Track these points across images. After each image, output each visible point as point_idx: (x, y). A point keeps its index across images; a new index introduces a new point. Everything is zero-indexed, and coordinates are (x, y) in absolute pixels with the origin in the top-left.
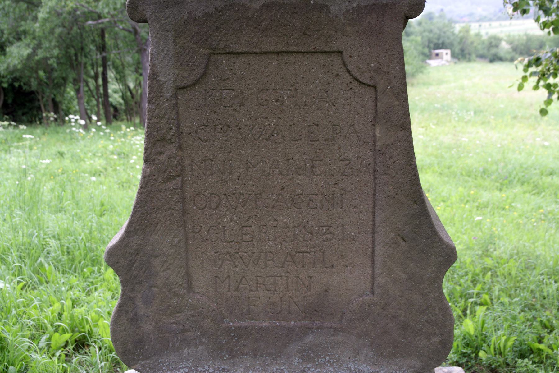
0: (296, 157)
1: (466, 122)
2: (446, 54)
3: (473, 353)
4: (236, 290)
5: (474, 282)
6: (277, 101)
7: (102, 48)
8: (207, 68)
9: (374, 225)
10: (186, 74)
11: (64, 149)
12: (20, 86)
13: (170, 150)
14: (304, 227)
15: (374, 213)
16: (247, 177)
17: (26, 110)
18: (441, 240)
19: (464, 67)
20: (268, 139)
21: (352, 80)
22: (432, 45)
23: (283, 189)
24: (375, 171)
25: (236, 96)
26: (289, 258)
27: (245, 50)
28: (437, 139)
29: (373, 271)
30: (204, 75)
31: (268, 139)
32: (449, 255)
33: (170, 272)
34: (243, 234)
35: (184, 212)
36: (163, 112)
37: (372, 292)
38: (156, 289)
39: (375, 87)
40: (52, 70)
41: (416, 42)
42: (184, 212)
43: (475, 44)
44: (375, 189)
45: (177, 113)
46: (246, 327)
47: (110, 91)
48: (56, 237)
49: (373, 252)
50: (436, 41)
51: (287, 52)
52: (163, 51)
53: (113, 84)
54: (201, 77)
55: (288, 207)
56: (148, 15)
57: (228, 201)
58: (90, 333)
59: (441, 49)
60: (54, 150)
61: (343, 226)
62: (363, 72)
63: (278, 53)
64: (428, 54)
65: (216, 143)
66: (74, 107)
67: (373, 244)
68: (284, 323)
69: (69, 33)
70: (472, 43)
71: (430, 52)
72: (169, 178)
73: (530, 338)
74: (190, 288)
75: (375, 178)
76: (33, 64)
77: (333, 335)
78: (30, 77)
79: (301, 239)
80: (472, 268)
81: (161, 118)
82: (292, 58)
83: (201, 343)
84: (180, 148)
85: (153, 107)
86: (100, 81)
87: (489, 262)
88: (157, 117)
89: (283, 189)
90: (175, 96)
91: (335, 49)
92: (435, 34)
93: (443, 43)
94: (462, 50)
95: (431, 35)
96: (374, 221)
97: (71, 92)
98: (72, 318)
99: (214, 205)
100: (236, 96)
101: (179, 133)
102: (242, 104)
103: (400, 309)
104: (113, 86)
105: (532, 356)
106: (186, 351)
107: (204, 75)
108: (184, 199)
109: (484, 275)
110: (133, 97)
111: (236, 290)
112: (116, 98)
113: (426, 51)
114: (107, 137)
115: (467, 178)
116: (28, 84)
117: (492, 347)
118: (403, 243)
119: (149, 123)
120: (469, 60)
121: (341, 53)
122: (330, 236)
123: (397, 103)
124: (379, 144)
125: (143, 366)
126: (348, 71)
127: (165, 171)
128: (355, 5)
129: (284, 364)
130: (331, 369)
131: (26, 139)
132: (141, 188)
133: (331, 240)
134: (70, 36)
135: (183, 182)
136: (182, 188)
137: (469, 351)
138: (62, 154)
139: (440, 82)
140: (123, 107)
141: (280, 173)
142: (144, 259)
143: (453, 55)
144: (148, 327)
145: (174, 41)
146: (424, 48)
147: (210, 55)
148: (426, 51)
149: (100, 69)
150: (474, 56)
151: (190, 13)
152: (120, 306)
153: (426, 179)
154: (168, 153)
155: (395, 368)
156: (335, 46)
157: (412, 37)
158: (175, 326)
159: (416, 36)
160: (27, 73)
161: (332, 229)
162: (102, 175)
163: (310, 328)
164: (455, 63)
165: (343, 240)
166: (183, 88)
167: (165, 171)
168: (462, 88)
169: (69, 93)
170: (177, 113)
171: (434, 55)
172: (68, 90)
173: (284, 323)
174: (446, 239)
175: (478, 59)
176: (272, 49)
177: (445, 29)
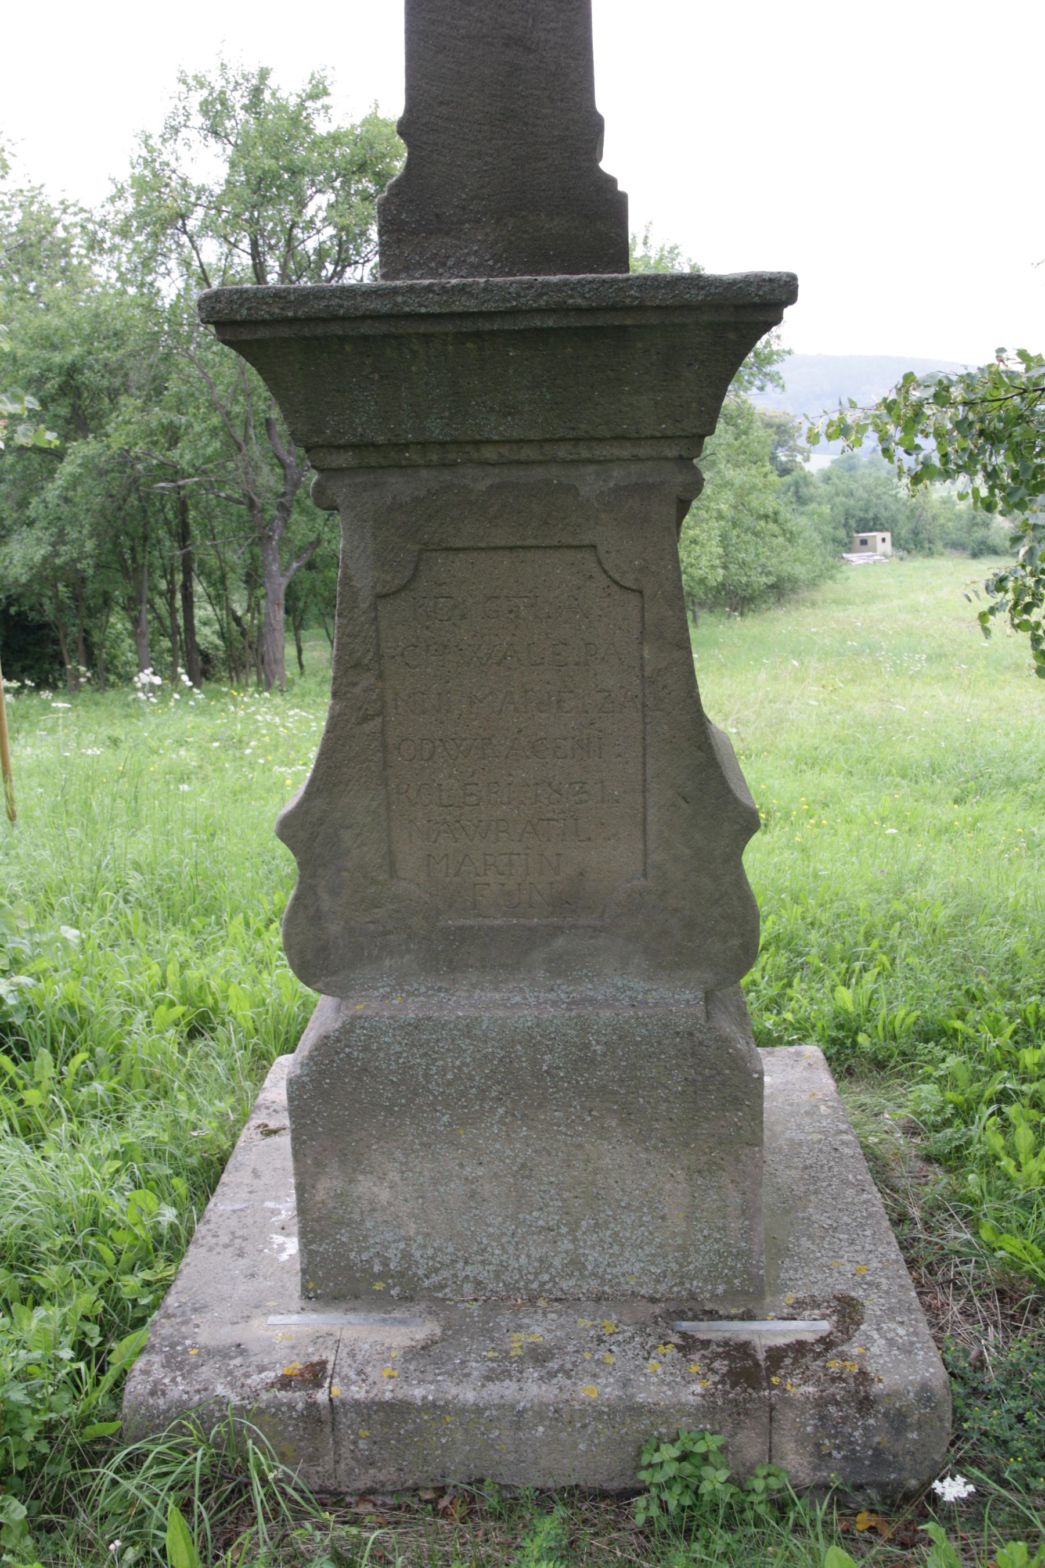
0: (538, 688)
1: (911, 677)
2: (881, 541)
3: (847, 1037)
4: (457, 874)
5: (868, 937)
6: (510, 612)
7: (183, 535)
8: (416, 568)
9: (645, 780)
10: (388, 578)
11: (119, 732)
12: (19, 614)
13: (367, 680)
14: (550, 784)
15: (644, 763)
16: (473, 716)
17: (28, 662)
18: (736, 800)
19: (917, 566)
20: (499, 664)
21: (610, 583)
22: (852, 523)
23: (520, 731)
24: (644, 705)
25: (455, 607)
26: (529, 828)
27: (467, 545)
28: (850, 708)
29: (645, 845)
30: (413, 578)
31: (499, 664)
32: (748, 823)
33: (365, 849)
34: (466, 795)
35: (386, 766)
36: (358, 628)
37: (645, 876)
38: (345, 874)
39: (641, 592)
40: (83, 580)
41: (820, 515)
42: (386, 766)
43: (942, 521)
44: (644, 731)
45: (377, 630)
46: (472, 927)
47: (196, 622)
48: (137, 867)
49: (645, 819)
50: (861, 514)
51: (523, 547)
52: (358, 547)
53: (200, 608)
54: (409, 582)
55: (528, 757)
56: (339, 501)
57: (445, 749)
58: (215, 1009)
59: (871, 531)
60: (105, 732)
61: (602, 782)
62: (624, 573)
63: (511, 549)
64: (846, 540)
65: (429, 670)
66: (123, 654)
67: (644, 807)
68: (523, 921)
69: (120, 509)
70: (935, 518)
71: (849, 536)
72: (366, 718)
73: (941, 1011)
74: (393, 872)
75: (645, 716)
76: (49, 572)
77: (591, 937)
78: (41, 595)
79: (546, 802)
80: (868, 916)
81: (356, 637)
82: (530, 555)
83: (408, 951)
84: (380, 676)
85: (345, 621)
86: (179, 603)
87: (899, 906)
88: (349, 636)
89: (520, 731)
90: (374, 607)
91: (586, 542)
92: (860, 499)
93: (876, 519)
94: (916, 533)
95: (852, 502)
96: (644, 775)
97: (118, 623)
98: (184, 986)
99: (426, 755)
100: (455, 607)
101: (379, 656)
102: (463, 617)
103: (683, 899)
104: (203, 611)
105: (943, 1040)
106: (387, 963)
107: (413, 578)
108: (385, 747)
109: (888, 927)
110: (243, 633)
111: (457, 874)
112: (207, 636)
113: (842, 533)
114: (203, 711)
115: (898, 779)
116: (39, 608)
117: (880, 1028)
118: (684, 805)
119: (339, 643)
120: (931, 554)
121: (595, 547)
122: (585, 797)
123: (670, 613)
124: (648, 669)
125: (327, 985)
126: (605, 572)
127: (360, 708)
128: (611, 485)
129: (524, 979)
130: (590, 986)
131: (56, 710)
132: (328, 732)
133: (586, 801)
134: (122, 513)
135: (384, 724)
136: (382, 732)
137: (841, 1034)
138: (115, 742)
139: (870, 598)
140: (221, 654)
141: (516, 710)
142: (330, 830)
143: (896, 543)
144: (334, 928)
145: (373, 534)
146: (835, 528)
147: (421, 551)
148: (842, 533)
149: (179, 578)
150: (939, 545)
151: (394, 498)
152: (297, 898)
153: (706, 710)
154: (364, 683)
155: (679, 984)
156: (587, 538)
157: (812, 507)
158: (372, 926)
159: (820, 504)
160: (36, 587)
161: (587, 787)
162: (193, 777)
163: (560, 928)
164: (901, 559)
165: (603, 802)
166: (385, 596)
167: (360, 708)
168: (915, 610)
169: (113, 626)
170: (377, 630)
171: (858, 542)
172: (112, 620)
173: (523, 921)
174: (744, 800)
175: (948, 552)
176: (502, 543)
177: (880, 490)
